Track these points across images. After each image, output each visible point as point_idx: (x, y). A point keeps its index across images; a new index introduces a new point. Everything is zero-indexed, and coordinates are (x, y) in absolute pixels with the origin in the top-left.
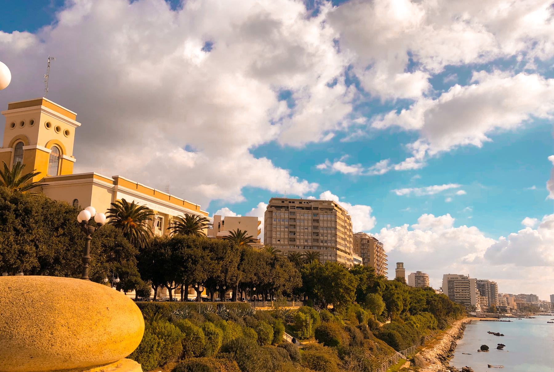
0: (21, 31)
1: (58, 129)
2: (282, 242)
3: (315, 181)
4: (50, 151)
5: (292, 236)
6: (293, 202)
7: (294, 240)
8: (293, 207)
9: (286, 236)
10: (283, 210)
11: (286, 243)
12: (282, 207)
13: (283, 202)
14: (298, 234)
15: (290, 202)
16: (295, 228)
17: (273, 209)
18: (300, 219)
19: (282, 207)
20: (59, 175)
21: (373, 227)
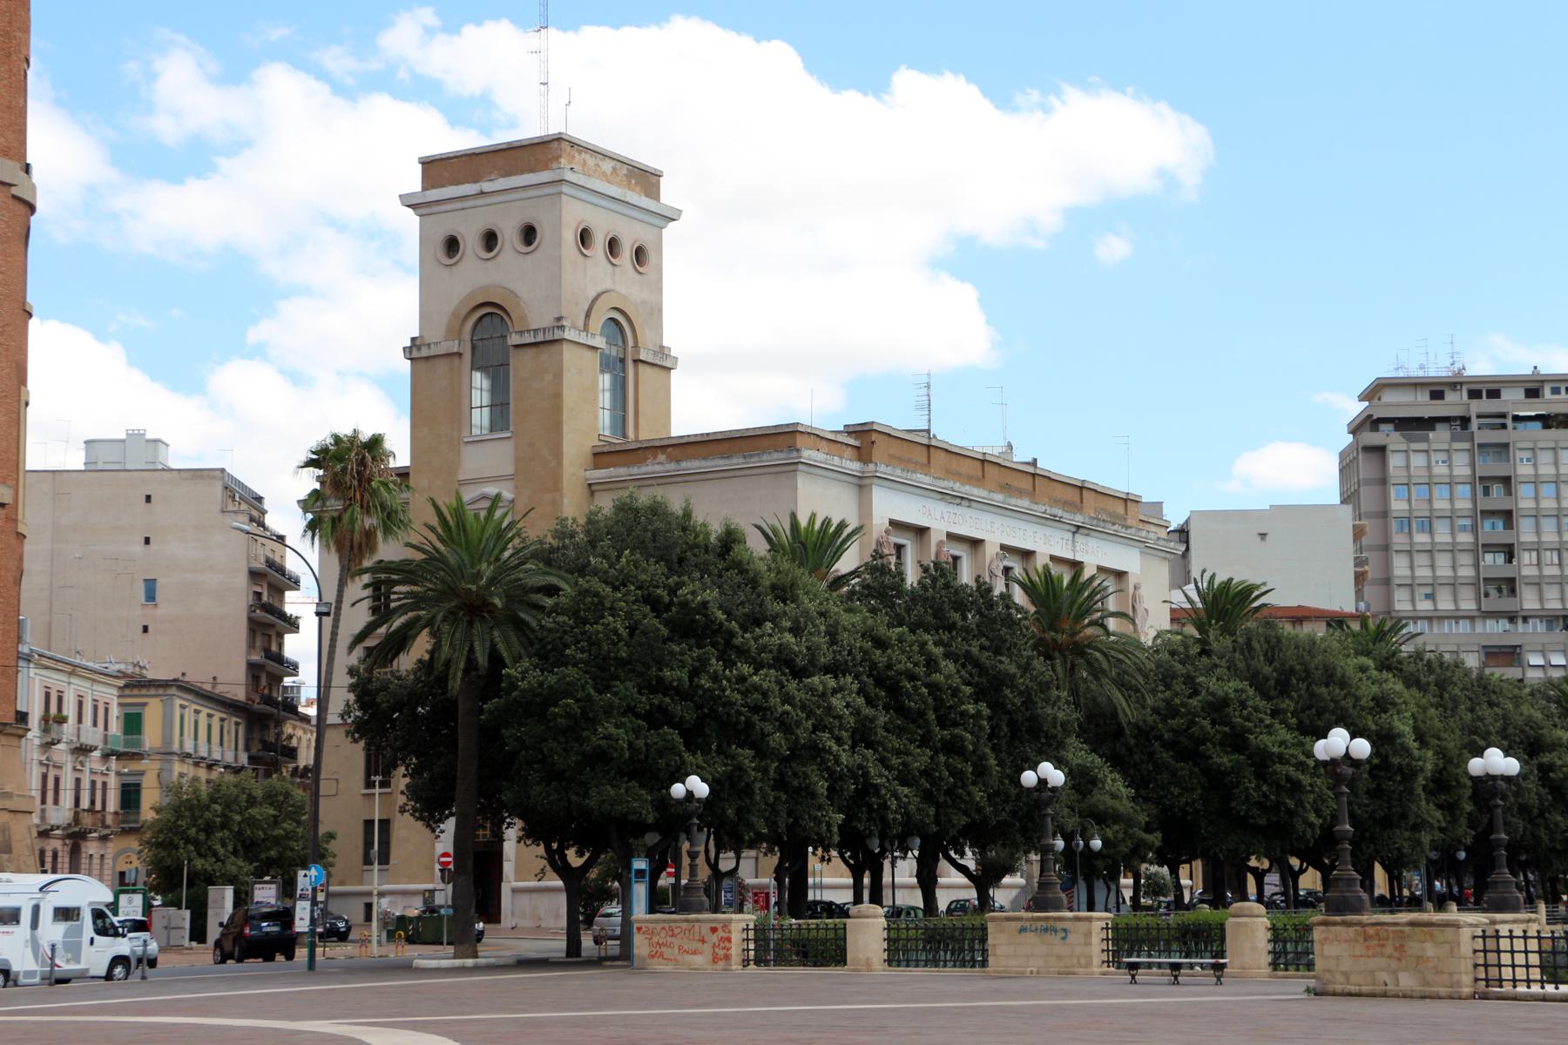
0: (969, 80)
1: (613, 246)
2: (1445, 604)
3: (679, 802)
4: (600, 342)
5: (1493, 531)
6: (1494, 394)
7: (1509, 586)
8: (1499, 420)
9: (1466, 572)
10: (1441, 435)
11: (1468, 605)
12: (1429, 423)
13: (1437, 395)
14: (1527, 558)
15: (1475, 394)
16: (1513, 591)
17: (1387, 436)
18: (1536, 481)
19: (1429, 423)
20: (631, 434)
21: (505, 23)
